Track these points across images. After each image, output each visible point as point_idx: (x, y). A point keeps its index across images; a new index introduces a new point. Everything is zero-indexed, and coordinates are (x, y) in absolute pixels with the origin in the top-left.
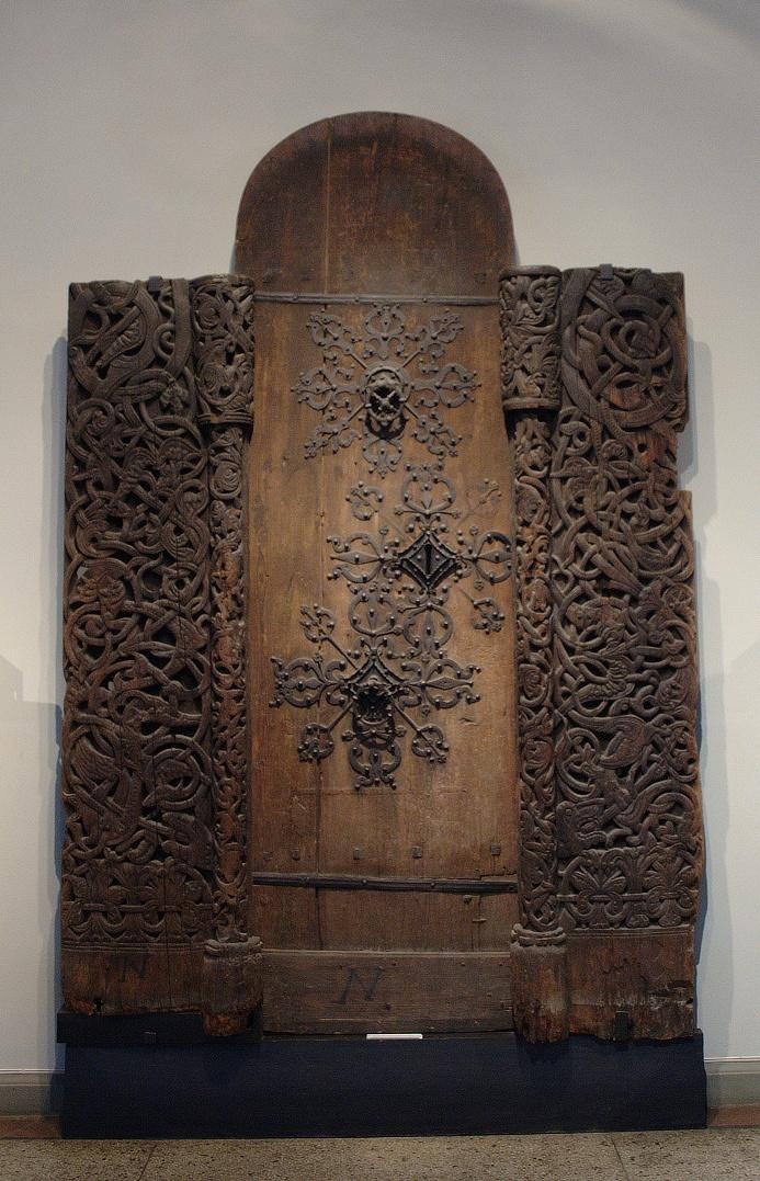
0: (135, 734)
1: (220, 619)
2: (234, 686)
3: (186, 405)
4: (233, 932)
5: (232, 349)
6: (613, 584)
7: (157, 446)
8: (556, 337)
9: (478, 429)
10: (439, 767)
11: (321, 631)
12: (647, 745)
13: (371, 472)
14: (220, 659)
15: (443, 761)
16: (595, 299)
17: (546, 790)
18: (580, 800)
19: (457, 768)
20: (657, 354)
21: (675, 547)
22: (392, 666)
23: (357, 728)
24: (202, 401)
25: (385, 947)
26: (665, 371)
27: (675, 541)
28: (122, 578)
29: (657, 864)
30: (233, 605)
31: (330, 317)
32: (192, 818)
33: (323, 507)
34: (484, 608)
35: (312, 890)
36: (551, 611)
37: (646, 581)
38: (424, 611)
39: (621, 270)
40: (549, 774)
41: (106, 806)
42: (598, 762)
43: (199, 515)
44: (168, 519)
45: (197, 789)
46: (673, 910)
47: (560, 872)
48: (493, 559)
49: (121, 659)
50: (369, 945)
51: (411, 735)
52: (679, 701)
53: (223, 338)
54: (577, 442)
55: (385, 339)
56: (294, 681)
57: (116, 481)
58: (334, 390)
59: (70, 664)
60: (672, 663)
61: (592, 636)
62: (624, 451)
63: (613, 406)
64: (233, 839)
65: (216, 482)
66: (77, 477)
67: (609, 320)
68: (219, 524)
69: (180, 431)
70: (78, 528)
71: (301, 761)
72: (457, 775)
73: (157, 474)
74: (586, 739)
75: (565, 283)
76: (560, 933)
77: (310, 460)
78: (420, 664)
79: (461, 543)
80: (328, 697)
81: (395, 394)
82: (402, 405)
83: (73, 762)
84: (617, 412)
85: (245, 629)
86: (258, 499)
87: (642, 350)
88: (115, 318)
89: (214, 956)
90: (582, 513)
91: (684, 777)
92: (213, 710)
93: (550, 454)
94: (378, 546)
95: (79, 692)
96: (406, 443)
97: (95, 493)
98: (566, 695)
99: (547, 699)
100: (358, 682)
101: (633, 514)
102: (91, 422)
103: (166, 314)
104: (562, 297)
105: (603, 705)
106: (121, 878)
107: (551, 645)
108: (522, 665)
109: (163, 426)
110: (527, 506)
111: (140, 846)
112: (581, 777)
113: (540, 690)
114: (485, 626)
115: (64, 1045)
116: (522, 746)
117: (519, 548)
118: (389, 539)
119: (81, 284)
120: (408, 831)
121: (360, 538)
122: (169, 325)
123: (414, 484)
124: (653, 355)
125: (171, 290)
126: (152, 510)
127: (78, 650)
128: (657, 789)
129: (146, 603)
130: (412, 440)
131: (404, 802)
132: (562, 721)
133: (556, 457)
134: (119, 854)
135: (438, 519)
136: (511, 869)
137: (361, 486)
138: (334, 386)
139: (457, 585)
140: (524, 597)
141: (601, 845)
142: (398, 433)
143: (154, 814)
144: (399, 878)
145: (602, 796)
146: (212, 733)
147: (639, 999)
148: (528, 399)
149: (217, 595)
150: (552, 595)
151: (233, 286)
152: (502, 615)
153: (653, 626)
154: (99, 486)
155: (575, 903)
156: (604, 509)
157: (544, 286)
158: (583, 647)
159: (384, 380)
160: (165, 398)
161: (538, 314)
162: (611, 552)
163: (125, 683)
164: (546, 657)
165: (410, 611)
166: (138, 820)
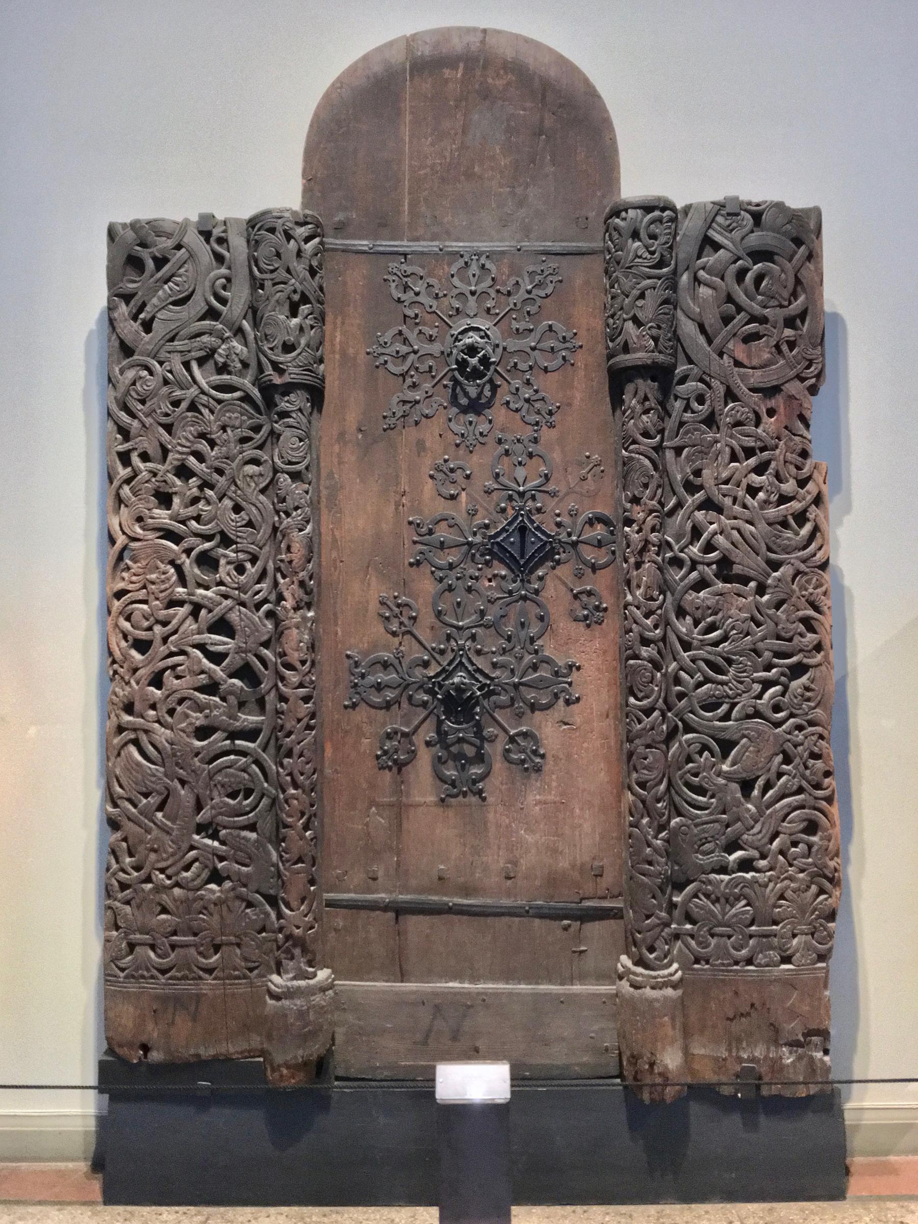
0: (188, 740)
1: (285, 608)
2: (301, 685)
3: (245, 365)
4: (300, 969)
5: (296, 297)
6: (737, 569)
7: (212, 412)
8: (673, 285)
9: (578, 395)
10: (533, 775)
11: (401, 623)
12: (777, 754)
13: (457, 445)
14: (285, 654)
15: (538, 769)
16: (718, 238)
17: (659, 805)
18: (698, 817)
19: (554, 777)
20: (790, 304)
21: (808, 527)
22: (480, 662)
23: (439, 731)
24: (262, 357)
25: (474, 979)
26: (798, 322)
27: (808, 520)
28: (172, 563)
29: (789, 894)
30: (300, 593)
31: (410, 269)
32: (253, 836)
33: (404, 486)
34: (584, 598)
35: (391, 915)
36: (664, 600)
37: (775, 566)
38: (517, 601)
39: (750, 204)
40: (662, 787)
41: (155, 824)
42: (719, 774)
43: (263, 491)
44: (225, 495)
45: (260, 802)
46: (808, 947)
47: (675, 899)
48: (596, 543)
49: (172, 654)
50: (454, 978)
51: (502, 739)
52: (812, 704)
53: (285, 283)
54: (695, 405)
55: (473, 293)
56: (371, 679)
57: (165, 452)
58: (415, 352)
59: (114, 662)
60: (806, 661)
61: (712, 628)
62: (751, 415)
63: (738, 364)
64: (300, 860)
65: (280, 451)
66: (121, 448)
67: (735, 262)
68: (283, 500)
69: (238, 394)
70: (122, 506)
71: (380, 769)
72: (554, 784)
73: (212, 444)
74: (705, 747)
75: (683, 223)
76: (676, 971)
77: (389, 431)
78: (513, 660)
79: (559, 525)
80: (410, 698)
81: (484, 355)
82: (492, 368)
83: (118, 772)
84: (742, 370)
85: (314, 620)
86: (330, 475)
87: (772, 298)
88: (160, 262)
89: (276, 997)
90: (701, 487)
91: (820, 793)
92: (278, 713)
93: (663, 420)
94: (465, 528)
95: (123, 692)
96: (498, 413)
97: (141, 466)
98: (681, 696)
99: (661, 701)
100: (444, 680)
101: (760, 489)
102: (134, 384)
103: (219, 259)
104: (678, 238)
105: (725, 707)
106: (170, 905)
107: (664, 639)
108: (631, 662)
109: (218, 388)
110: (637, 478)
111: (193, 869)
112: (701, 791)
113: (653, 690)
114: (586, 618)
115: (107, 1096)
116: (630, 755)
117: (627, 529)
118: (478, 521)
119: (120, 224)
120: (499, 849)
121: (447, 520)
122: (223, 271)
123: (506, 459)
124: (786, 303)
125: (225, 231)
126: (206, 484)
127: (124, 644)
128: (789, 805)
129: (201, 591)
130: (503, 410)
131: (495, 815)
132: (676, 726)
133: (670, 424)
134: (169, 878)
135: (533, 498)
136: (616, 892)
137: (446, 461)
138: (416, 347)
139: (555, 571)
140: (634, 583)
141: (723, 870)
142: (489, 404)
143: (210, 832)
144: (489, 901)
145: (724, 813)
146: (277, 739)
147: (768, 1049)
148: (640, 355)
149: (282, 581)
150: (665, 581)
151: (297, 223)
152: (605, 605)
153: (784, 617)
154: (145, 457)
155: (692, 937)
156: (726, 482)
157: (660, 220)
158: (701, 641)
159: (472, 338)
160: (220, 355)
161: (653, 253)
162: (735, 533)
163: (176, 682)
164: (659, 652)
165: (502, 601)
166: (191, 839)
